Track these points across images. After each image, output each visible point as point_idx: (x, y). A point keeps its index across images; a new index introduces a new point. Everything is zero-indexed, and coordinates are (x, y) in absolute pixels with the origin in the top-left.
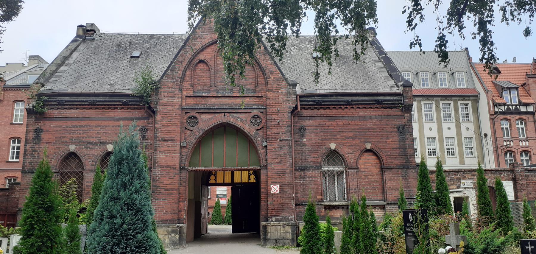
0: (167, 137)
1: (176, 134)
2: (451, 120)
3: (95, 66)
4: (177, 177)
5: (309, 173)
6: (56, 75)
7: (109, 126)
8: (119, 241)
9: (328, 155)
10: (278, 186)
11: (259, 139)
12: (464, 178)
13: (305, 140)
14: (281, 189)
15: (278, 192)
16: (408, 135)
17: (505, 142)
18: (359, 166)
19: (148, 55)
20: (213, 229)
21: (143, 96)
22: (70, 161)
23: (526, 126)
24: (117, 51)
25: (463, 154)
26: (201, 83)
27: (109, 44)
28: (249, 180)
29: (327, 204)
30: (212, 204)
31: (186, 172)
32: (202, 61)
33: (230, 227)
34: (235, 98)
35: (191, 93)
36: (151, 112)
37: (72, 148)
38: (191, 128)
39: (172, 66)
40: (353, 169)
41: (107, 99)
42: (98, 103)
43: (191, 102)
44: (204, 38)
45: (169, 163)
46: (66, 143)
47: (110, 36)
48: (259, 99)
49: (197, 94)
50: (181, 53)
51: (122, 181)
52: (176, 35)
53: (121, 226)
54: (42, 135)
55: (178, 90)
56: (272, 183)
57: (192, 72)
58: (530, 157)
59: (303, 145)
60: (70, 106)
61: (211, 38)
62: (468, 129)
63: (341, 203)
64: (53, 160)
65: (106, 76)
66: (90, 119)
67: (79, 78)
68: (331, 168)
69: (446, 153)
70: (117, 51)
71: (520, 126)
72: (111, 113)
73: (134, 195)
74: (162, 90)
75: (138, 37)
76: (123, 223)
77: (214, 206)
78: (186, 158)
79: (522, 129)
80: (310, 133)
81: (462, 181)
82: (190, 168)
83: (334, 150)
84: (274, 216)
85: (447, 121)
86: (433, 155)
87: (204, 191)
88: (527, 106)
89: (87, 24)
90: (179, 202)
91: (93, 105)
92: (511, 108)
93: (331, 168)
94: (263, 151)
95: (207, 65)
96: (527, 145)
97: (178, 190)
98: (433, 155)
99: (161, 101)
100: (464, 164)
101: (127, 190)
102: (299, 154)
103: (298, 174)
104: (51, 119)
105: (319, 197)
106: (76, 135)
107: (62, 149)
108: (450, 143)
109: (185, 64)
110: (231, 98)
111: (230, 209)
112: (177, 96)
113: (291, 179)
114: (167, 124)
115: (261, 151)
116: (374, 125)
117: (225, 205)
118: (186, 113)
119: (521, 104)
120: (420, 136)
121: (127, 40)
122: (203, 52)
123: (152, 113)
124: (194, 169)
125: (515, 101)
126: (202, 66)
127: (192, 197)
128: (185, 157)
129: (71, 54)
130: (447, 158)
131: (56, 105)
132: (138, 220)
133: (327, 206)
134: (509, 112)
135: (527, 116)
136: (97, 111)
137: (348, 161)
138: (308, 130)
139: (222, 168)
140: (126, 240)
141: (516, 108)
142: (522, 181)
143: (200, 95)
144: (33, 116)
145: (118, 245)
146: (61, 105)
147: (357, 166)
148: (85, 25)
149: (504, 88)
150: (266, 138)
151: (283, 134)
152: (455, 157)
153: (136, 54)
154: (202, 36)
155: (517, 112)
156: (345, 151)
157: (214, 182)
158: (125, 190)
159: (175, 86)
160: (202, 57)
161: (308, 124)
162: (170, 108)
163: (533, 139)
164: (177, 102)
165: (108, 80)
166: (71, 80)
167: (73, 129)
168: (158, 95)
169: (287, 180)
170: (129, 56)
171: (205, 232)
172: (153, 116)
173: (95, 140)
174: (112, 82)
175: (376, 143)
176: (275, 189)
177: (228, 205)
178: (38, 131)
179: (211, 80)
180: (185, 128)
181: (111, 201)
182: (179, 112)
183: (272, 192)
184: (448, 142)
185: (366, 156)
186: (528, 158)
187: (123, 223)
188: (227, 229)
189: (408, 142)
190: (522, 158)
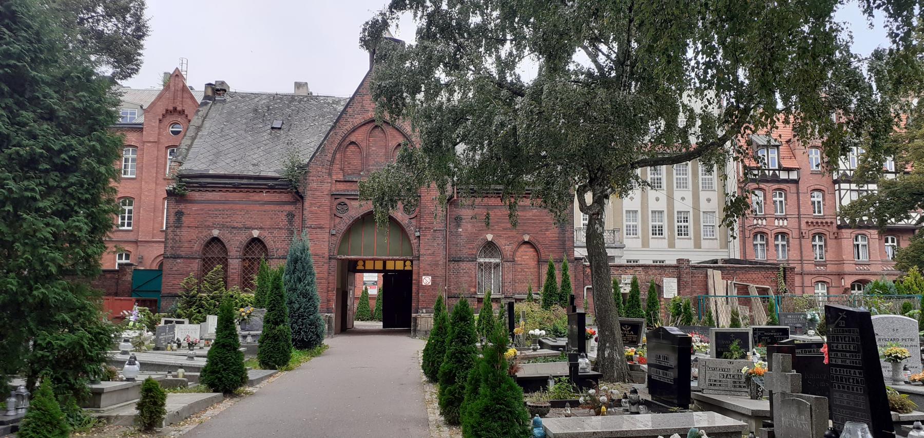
1: (325, 221)
2: (686, 187)
3: (232, 140)
4: (326, 266)
5: (463, 265)
6: (192, 150)
7: (254, 210)
8: (297, 320)
9: (485, 247)
10: (430, 277)
11: (412, 228)
12: (626, 273)
13: (461, 230)
14: (433, 281)
15: (430, 284)
16: (568, 227)
17: (755, 221)
18: (516, 259)
19: (291, 125)
20: (358, 324)
21: (291, 181)
22: (213, 246)
23: (786, 199)
24: (254, 119)
25: (700, 235)
27: (244, 109)
28: (404, 267)
29: (480, 296)
30: (359, 294)
31: (335, 261)
32: (352, 143)
33: (381, 324)
35: (341, 178)
36: (299, 198)
37: (216, 233)
38: (341, 215)
39: (321, 148)
40: (509, 262)
41: (252, 181)
42: (242, 186)
43: (341, 187)
46: (209, 228)
47: (245, 96)
49: (347, 179)
50: (331, 134)
51: (298, 276)
52: (321, 96)
53: (299, 309)
54: (184, 218)
56: (424, 275)
58: (788, 242)
59: (458, 235)
60: (213, 188)
61: (364, 118)
62: (709, 200)
63: (498, 297)
64: (196, 245)
65: (247, 153)
66: (233, 202)
67: (218, 154)
68: (487, 260)
69: (676, 233)
70: (254, 119)
71: (778, 199)
72: (256, 197)
73: (307, 287)
74: (311, 174)
75: (277, 99)
76: (300, 307)
77: (360, 296)
79: (781, 202)
80: (466, 223)
81: (623, 276)
82: (338, 257)
83: (491, 242)
84: (425, 308)
85: (682, 189)
86: (659, 234)
87: (350, 278)
88: (790, 172)
89: (216, 82)
90: (328, 291)
91: (236, 187)
92: (767, 174)
93: (487, 260)
94: (416, 241)
95: (358, 147)
96: (786, 224)
97: (327, 279)
98: (659, 234)
99: (309, 186)
100: (700, 248)
101: (302, 283)
102: (453, 245)
103: (452, 265)
104: (192, 202)
105: (473, 290)
106: (219, 220)
107: (205, 234)
108: (683, 219)
109: (334, 146)
111: (381, 301)
112: (326, 181)
113: (444, 271)
115: (414, 241)
116: (533, 216)
117: (375, 295)
118: (335, 199)
119: (781, 168)
120: (642, 208)
121: (264, 103)
122: (354, 133)
123: (299, 198)
124: (343, 257)
125: (774, 165)
126: (352, 148)
127: (339, 287)
129: (203, 121)
130: (678, 238)
131: (198, 187)
132: (310, 305)
133: (480, 298)
134: (764, 179)
135: (788, 185)
136: (241, 193)
137: (504, 253)
138: (465, 219)
139: (372, 257)
140: (302, 319)
141: (774, 174)
142: (686, 278)
143: (350, 179)
144: (173, 198)
145: (296, 323)
146: (203, 187)
147: (514, 259)
148: (214, 83)
149: (760, 145)
150: (420, 228)
151: (438, 224)
152: (688, 239)
153: (277, 124)
155: (776, 180)
156: (502, 243)
157: (363, 268)
158: (300, 283)
159: (324, 170)
160: (353, 138)
161: (466, 213)
162: (318, 193)
163: (794, 216)
164: (326, 187)
165: (250, 158)
166: (210, 158)
167: (216, 212)
168: (306, 179)
169: (440, 271)
170: (270, 126)
171: (350, 327)
172: (301, 201)
173: (240, 225)
174: (255, 162)
175: (535, 235)
176: (427, 280)
177: (379, 295)
178: (179, 214)
179: (362, 164)
180: (335, 215)
181: (289, 291)
182: (328, 198)
183: (423, 284)
184: (681, 218)
185: (524, 248)
186: (785, 243)
187: (300, 307)
188: (379, 325)
189: (568, 234)
190: (776, 243)
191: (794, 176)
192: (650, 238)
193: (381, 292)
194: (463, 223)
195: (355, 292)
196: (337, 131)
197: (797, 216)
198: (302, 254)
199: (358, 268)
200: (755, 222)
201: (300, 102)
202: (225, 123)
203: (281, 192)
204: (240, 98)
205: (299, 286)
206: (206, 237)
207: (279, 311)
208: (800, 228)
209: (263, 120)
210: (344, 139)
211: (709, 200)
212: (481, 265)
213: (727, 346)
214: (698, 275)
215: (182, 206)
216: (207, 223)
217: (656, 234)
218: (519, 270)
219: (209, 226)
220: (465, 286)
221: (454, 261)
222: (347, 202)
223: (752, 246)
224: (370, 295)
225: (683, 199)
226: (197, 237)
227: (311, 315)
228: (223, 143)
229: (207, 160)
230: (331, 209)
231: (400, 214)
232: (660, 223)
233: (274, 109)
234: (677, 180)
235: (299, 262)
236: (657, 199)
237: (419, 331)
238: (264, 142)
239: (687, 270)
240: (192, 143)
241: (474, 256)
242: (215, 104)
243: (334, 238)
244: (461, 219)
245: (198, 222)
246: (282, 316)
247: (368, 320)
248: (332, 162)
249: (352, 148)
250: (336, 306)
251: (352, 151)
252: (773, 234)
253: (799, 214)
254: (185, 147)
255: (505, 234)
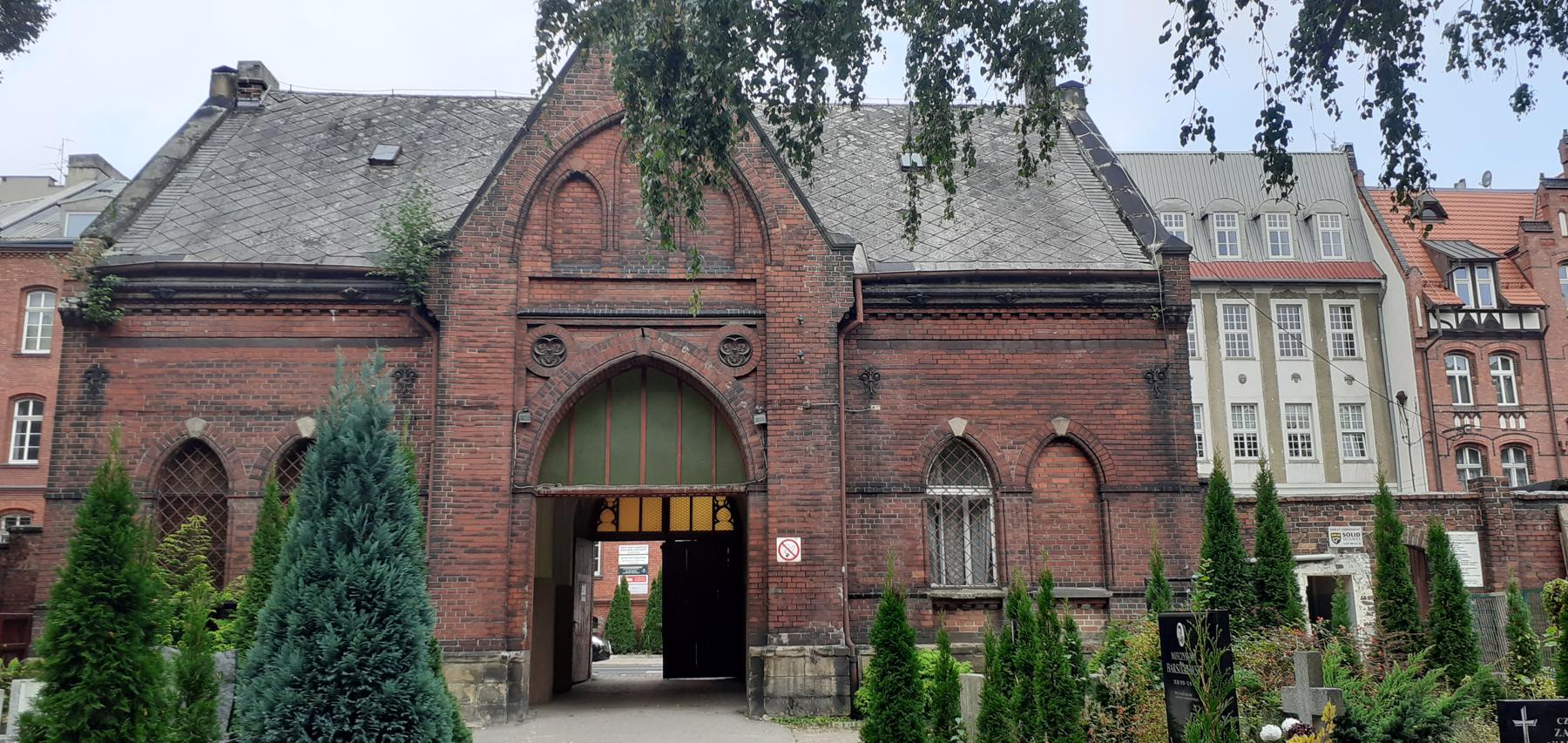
0: (473, 398)
1: (500, 386)
2: (1301, 353)
3: (263, 189)
4: (503, 514)
5: (889, 505)
8: (332, 698)
9: (944, 454)
10: (798, 540)
11: (744, 404)
12: (1339, 521)
13: (877, 408)
14: (807, 550)
15: (799, 559)
18: (1035, 486)
19: (421, 156)
22: (188, 465)
23: (1518, 373)
24: (329, 144)
25: (1337, 453)
26: (574, 241)
27: (305, 124)
28: (714, 523)
29: (940, 593)
30: (604, 592)
32: (577, 177)
33: (658, 661)
34: (676, 285)
35: (545, 269)
36: (429, 324)
37: (196, 427)
38: (545, 372)
39: (489, 190)
41: (299, 283)
43: (546, 296)
44: (583, 109)
45: (479, 472)
48: (745, 287)
49: (562, 273)
50: (516, 151)
51: (341, 524)
52: (503, 98)
53: (339, 657)
54: (108, 389)
55: (506, 259)
56: (782, 533)
57: (550, 208)
58: (1530, 463)
59: (872, 421)
60: (192, 303)
61: (606, 108)
64: (140, 462)
66: (248, 341)
68: (953, 491)
70: (329, 144)
71: (1501, 372)
72: (311, 326)
73: (376, 565)
74: (461, 260)
75: (392, 105)
76: (344, 648)
78: (530, 459)
79: (1508, 380)
80: (893, 387)
81: (1331, 530)
82: (540, 488)
83: (963, 439)
84: (786, 629)
85: (1292, 357)
89: (240, 63)
90: (509, 586)
91: (256, 302)
93: (953, 491)
94: (755, 439)
95: (593, 186)
96: (1523, 426)
97: (507, 550)
98: (1250, 454)
99: (456, 292)
100: (1340, 481)
101: (356, 551)
103: (856, 506)
104: (135, 342)
105: (918, 574)
106: (208, 390)
107: (165, 430)
109: (527, 185)
110: (664, 284)
111: (659, 608)
112: (503, 277)
113: (835, 521)
114: (474, 360)
115: (751, 440)
116: (1077, 366)
117: (644, 596)
118: (530, 326)
119: (1503, 307)
120: (1211, 399)
121: (359, 113)
122: (582, 151)
123: (429, 327)
124: (553, 489)
127: (548, 573)
128: (526, 456)
129: (194, 150)
131: (150, 301)
132: (388, 638)
134: (1468, 331)
135: (1520, 342)
136: (270, 318)
137: (1003, 470)
140: (353, 696)
141: (1491, 320)
142: (1504, 530)
143: (571, 273)
144: (81, 333)
145: (327, 710)
146: (164, 301)
148: (235, 67)
149: (1456, 260)
151: (815, 391)
153: (385, 153)
154: (580, 103)
155: (1493, 331)
156: (992, 441)
157: (612, 529)
158: (349, 550)
159: (497, 249)
160: (577, 163)
161: (888, 362)
164: (505, 294)
165: (301, 228)
166: (194, 229)
167: (199, 371)
168: (447, 274)
169: (825, 523)
170: (365, 160)
171: (583, 676)
173: (262, 405)
174: (313, 235)
176: (789, 549)
177: (652, 596)
178: (96, 377)
179: (605, 232)
180: (528, 371)
181: (308, 583)
182: (511, 323)
183: (779, 559)
184: (1294, 418)
185: (1055, 455)
186: (1523, 465)
187: (344, 648)
188: (649, 667)
189: (1175, 415)
190: (1505, 466)
191: (1532, 323)
192: (1232, 461)
193: (659, 589)
194: (884, 388)
195: (597, 588)
196: (535, 143)
197: (1546, 408)
198: (360, 439)
199: (602, 528)
200: (1457, 422)
201: (449, 110)
202: (251, 154)
203: (379, 311)
204: (300, 104)
205: (342, 562)
206: (168, 438)
207: (105, 687)
208: (1554, 433)
209: (351, 147)
210: (555, 163)
211: (1350, 379)
212: (933, 506)
213: (615, 603)
214: (1534, 522)
215: (104, 356)
216: (174, 401)
217: (1243, 454)
218: (1045, 516)
219: (176, 410)
220: (895, 564)
221: (863, 494)
222: (562, 334)
223: (1455, 474)
224: (634, 596)
225: (1296, 377)
226: (144, 440)
227: (386, 677)
228: (237, 196)
229: (185, 233)
230: (517, 355)
231: (708, 366)
232: (1251, 431)
233: (382, 124)
234: (1281, 338)
235: (349, 472)
236: (1243, 380)
237: (769, 696)
238: (345, 193)
239: (1506, 509)
240: (152, 196)
241: (917, 479)
242: (234, 116)
243: (526, 435)
244: (877, 378)
245: (149, 397)
246: (120, 716)
247: (629, 651)
248: (521, 226)
249: (576, 190)
250: (536, 627)
251: (574, 200)
252: (1497, 447)
253: (1550, 404)
254: (130, 203)
255: (1001, 417)
